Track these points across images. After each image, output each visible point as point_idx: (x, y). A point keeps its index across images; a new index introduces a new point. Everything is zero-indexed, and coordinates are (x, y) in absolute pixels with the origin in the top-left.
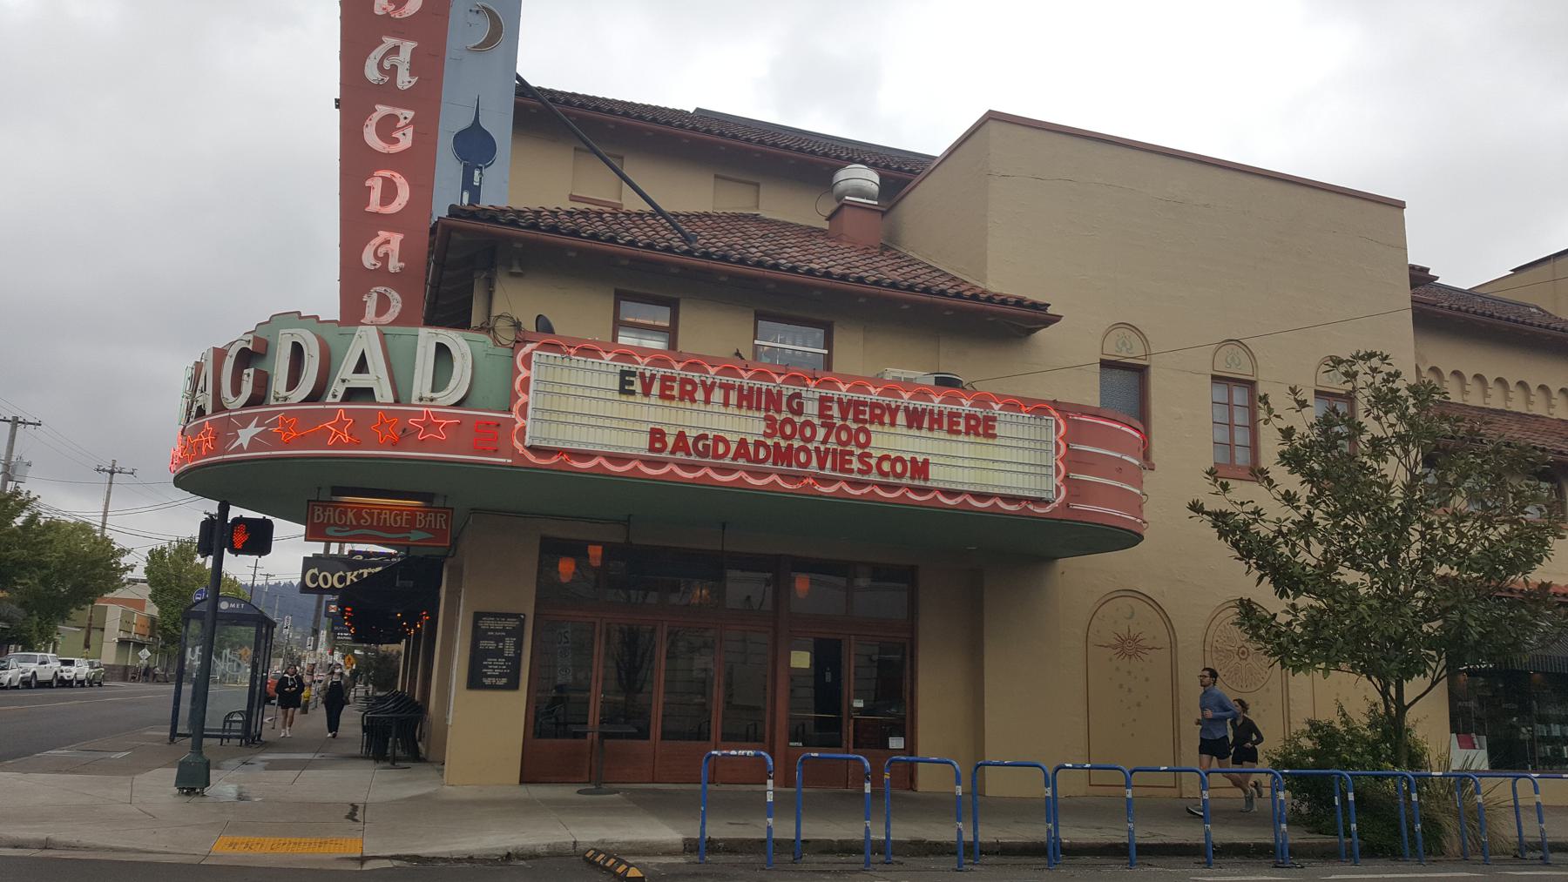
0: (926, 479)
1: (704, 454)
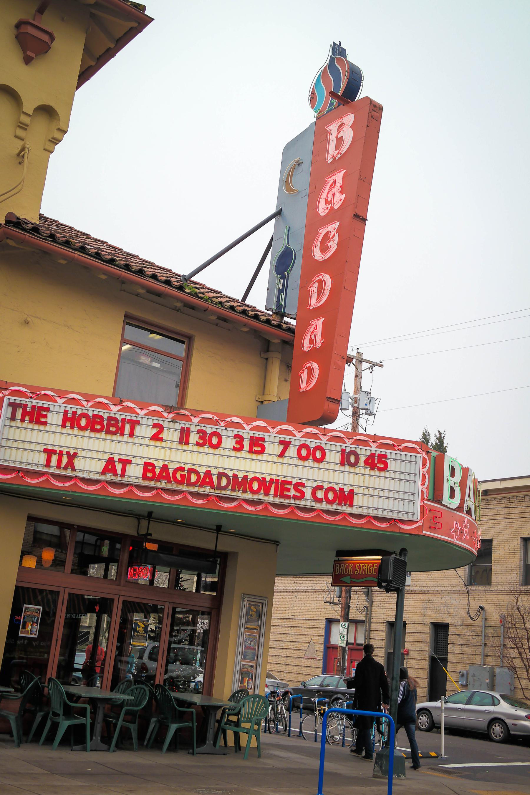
0: (351, 505)
1: (181, 483)
